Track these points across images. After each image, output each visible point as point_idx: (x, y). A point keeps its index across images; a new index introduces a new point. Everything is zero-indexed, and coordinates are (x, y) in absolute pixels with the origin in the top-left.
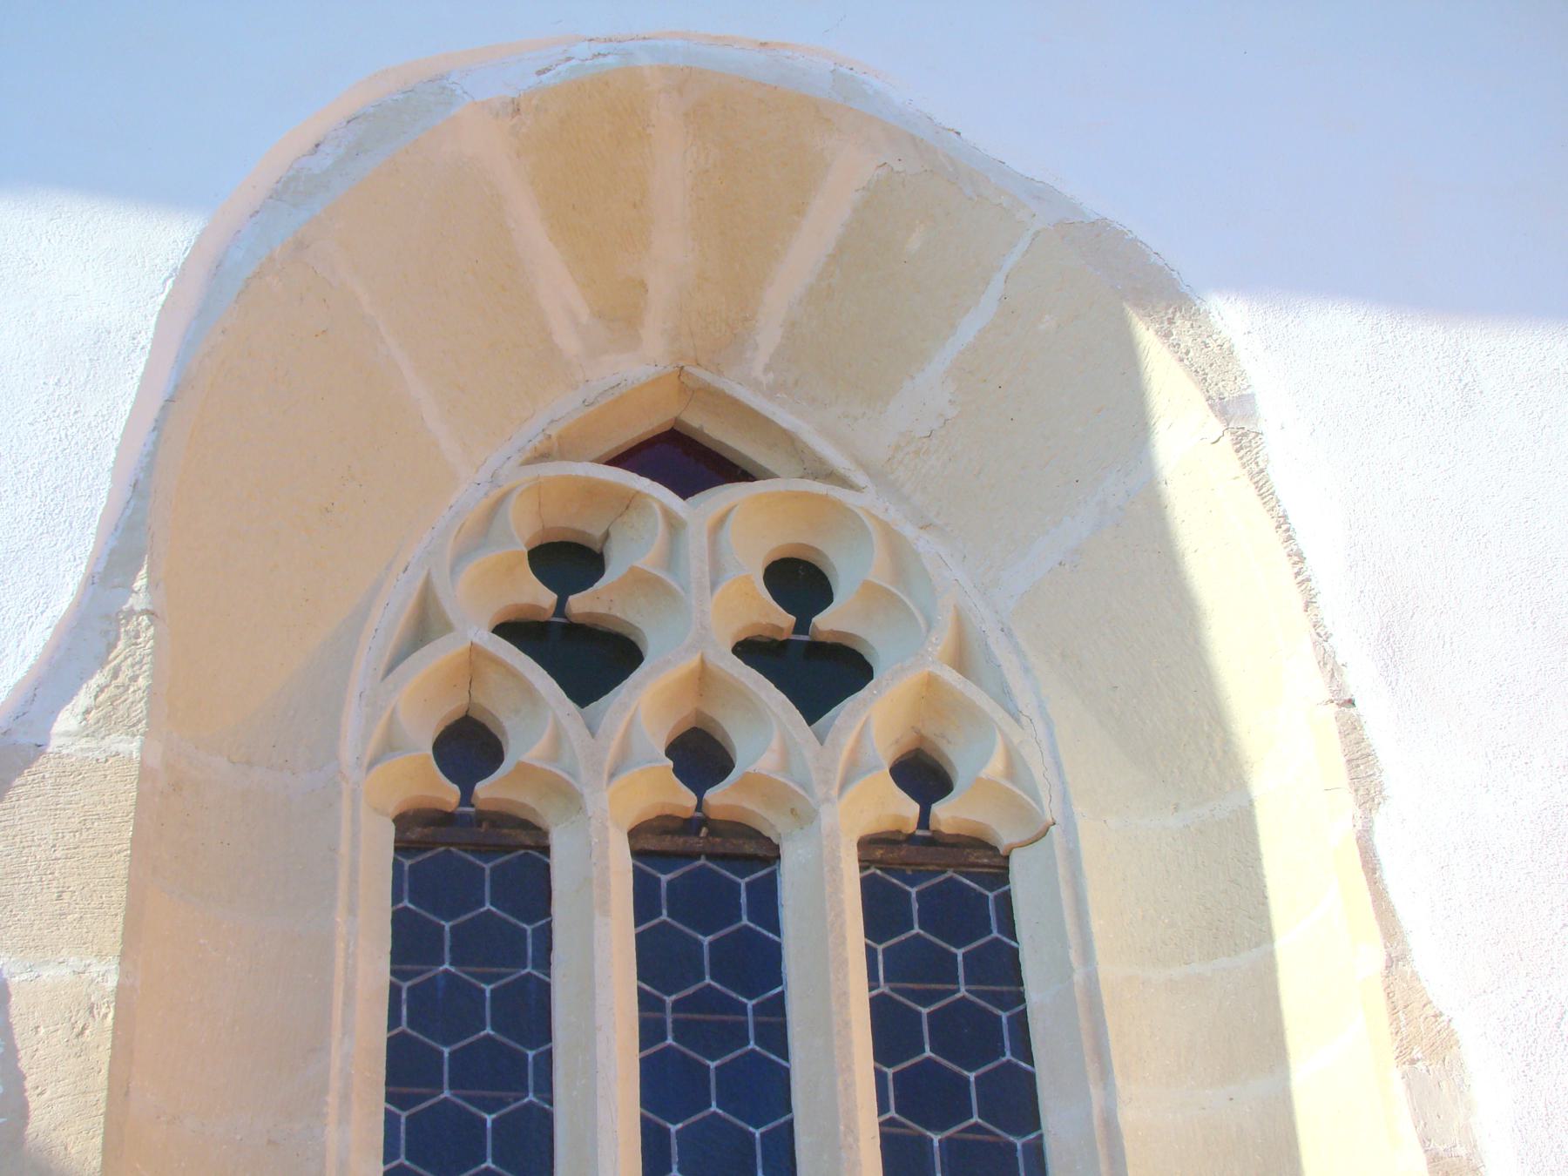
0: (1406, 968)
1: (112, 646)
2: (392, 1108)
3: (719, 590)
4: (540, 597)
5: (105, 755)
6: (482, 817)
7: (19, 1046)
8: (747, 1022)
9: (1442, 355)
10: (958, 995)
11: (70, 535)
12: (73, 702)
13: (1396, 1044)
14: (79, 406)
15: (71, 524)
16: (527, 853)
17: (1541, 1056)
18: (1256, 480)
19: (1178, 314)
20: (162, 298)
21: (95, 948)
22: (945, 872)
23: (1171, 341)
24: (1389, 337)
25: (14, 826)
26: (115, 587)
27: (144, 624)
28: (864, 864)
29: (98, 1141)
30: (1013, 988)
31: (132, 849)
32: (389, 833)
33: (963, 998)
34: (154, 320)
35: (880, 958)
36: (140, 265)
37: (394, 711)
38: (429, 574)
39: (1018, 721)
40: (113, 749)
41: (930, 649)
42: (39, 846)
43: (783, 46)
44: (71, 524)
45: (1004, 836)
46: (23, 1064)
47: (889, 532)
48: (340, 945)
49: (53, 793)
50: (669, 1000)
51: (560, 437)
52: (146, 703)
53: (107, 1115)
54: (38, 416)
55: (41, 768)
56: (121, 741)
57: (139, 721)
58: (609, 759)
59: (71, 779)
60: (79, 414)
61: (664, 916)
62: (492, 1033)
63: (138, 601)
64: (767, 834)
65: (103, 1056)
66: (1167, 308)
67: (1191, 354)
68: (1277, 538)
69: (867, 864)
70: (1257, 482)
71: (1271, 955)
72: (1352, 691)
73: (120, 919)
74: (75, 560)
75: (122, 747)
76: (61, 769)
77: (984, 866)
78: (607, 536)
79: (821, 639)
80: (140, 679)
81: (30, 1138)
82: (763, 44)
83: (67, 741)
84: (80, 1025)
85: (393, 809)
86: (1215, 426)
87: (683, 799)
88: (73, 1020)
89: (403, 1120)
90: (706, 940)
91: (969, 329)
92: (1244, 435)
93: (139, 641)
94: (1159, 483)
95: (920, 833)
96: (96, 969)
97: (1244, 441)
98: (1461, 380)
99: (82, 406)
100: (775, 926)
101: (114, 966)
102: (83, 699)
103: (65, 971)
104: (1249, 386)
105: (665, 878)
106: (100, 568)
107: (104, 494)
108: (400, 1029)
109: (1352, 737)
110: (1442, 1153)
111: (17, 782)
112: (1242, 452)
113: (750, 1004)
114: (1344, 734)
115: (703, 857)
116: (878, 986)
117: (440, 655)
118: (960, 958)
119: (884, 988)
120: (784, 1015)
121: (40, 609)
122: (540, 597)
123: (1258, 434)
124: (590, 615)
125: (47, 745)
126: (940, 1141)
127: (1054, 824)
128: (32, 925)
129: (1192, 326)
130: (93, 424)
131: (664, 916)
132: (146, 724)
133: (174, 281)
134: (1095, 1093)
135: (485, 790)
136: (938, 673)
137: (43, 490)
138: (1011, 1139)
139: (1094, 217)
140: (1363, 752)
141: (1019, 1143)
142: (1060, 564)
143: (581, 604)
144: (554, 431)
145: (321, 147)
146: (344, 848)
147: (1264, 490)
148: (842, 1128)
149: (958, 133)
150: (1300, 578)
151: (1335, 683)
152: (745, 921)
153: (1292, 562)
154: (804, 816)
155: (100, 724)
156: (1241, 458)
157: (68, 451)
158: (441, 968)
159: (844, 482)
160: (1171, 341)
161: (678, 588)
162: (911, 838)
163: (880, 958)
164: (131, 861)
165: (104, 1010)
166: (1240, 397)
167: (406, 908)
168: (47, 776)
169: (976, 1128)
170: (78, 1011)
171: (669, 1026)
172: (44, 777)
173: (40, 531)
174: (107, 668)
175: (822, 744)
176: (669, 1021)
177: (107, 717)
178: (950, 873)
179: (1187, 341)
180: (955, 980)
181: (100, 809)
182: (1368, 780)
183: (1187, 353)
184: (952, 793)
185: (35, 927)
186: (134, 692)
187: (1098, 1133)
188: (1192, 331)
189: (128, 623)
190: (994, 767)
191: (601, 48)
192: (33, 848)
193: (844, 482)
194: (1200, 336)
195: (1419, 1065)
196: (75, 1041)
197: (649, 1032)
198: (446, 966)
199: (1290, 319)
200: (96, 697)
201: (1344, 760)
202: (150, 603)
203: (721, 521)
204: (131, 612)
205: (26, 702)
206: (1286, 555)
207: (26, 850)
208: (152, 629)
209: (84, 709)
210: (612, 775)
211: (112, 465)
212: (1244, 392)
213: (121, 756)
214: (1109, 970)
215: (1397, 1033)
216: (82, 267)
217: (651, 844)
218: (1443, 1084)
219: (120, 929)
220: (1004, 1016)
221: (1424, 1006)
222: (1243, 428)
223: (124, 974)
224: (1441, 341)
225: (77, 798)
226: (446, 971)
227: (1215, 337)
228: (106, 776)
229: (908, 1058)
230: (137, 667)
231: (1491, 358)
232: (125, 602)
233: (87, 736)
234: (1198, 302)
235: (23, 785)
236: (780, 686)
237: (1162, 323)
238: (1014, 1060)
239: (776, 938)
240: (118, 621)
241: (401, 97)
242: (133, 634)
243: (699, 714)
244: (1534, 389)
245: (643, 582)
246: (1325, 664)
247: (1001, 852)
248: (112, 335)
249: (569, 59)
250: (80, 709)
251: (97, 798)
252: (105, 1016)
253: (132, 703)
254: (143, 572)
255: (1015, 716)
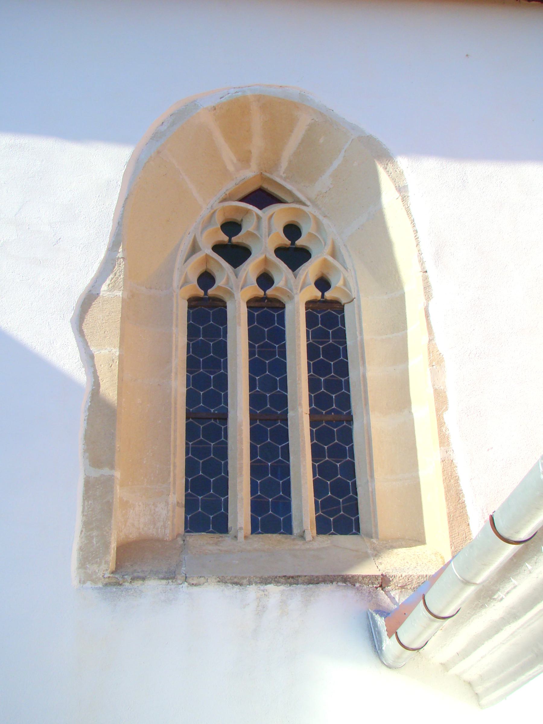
0: (434, 342)
1: (114, 267)
2: (188, 374)
3: (270, 236)
4: (224, 238)
5: (114, 296)
6: (210, 298)
7: (97, 370)
8: (276, 351)
9: (458, 172)
10: (330, 342)
11: (103, 238)
12: (105, 282)
13: (429, 362)
14: (104, 202)
15: (103, 235)
16: (221, 308)
17: (464, 363)
18: (407, 209)
19: (389, 162)
20: (124, 171)
21: (113, 345)
22: (328, 310)
23: (387, 170)
24: (445, 167)
25: (93, 315)
26: (114, 251)
27: (122, 261)
28: (307, 309)
29: (116, 392)
30: (344, 340)
31: (121, 320)
32: (186, 304)
33: (331, 343)
34: (122, 177)
35: (310, 333)
36: (118, 162)
37: (186, 274)
38: (195, 235)
39: (347, 270)
40: (115, 295)
41: (325, 251)
42: (99, 320)
43: (286, 87)
44: (103, 235)
45: (343, 301)
46: (98, 374)
47: (315, 217)
48: (174, 335)
49: (102, 306)
50: (257, 345)
51: (229, 194)
52: (123, 282)
53: (118, 386)
54: (94, 206)
55: (99, 300)
56: (117, 292)
57: (121, 287)
58: (241, 284)
59: (106, 303)
60: (104, 205)
61: (256, 324)
62: (212, 355)
63: (120, 255)
64: (282, 301)
65: (116, 372)
66: (387, 160)
67: (392, 174)
68: (411, 226)
69: (307, 308)
70: (407, 210)
71: (406, 333)
72: (427, 269)
73: (119, 338)
74: (104, 245)
75: (118, 294)
76: (103, 300)
77: (337, 308)
78: (242, 220)
79: (298, 247)
80: (121, 276)
81: (101, 392)
82: (281, 87)
83: (104, 292)
84: (111, 364)
85: (187, 298)
86: (397, 194)
87: (261, 293)
88: (109, 363)
89: (191, 377)
90: (266, 330)
91: (336, 164)
92: (405, 197)
93: (121, 265)
94: (383, 209)
95: (322, 299)
96: (114, 350)
97: (404, 199)
98: (463, 179)
99: (105, 202)
100: (284, 326)
101: (118, 350)
102: (108, 282)
103: (107, 351)
104: (407, 183)
105: (256, 314)
106: (111, 246)
107: (111, 226)
108: (190, 354)
109: (426, 281)
110: (437, 388)
111: (93, 303)
112: (404, 202)
113: (277, 346)
114: (423, 280)
115: (266, 308)
116: (309, 341)
117: (198, 257)
118: (331, 333)
119: (311, 341)
120: (286, 349)
121: (97, 259)
122: (224, 238)
123: (408, 196)
124: (238, 242)
125: (100, 294)
126: (323, 380)
127: (355, 298)
128: (99, 340)
129: (393, 166)
130: (108, 207)
131: (256, 324)
132: (123, 288)
133: (127, 166)
134: (361, 369)
135: (211, 292)
136: (327, 258)
137: (96, 226)
138: (341, 379)
139: (368, 135)
140: (428, 285)
141: (343, 380)
142: (359, 229)
143: (235, 239)
144: (227, 193)
145: (164, 123)
146: (174, 310)
147: (409, 212)
148: (297, 379)
149: (333, 111)
150: (416, 237)
151: (422, 267)
152: (276, 324)
153: (414, 233)
154: (291, 298)
155: (112, 288)
156: (403, 203)
157: (102, 215)
158: (200, 338)
159: (304, 204)
160: (387, 170)
161: (259, 236)
162: (319, 301)
163: (310, 333)
164: (121, 323)
165: (116, 361)
166: (404, 186)
167: (191, 323)
168: (100, 302)
169: (333, 376)
170: (110, 361)
171: (257, 352)
172: (99, 302)
173: (96, 237)
174: (113, 273)
175: (296, 278)
176: (257, 351)
177: (114, 286)
178: (329, 310)
179: (391, 170)
180: (329, 338)
181: (113, 310)
182: (429, 292)
183: (391, 174)
184: (331, 288)
185: (99, 340)
186: (120, 279)
187: (361, 378)
188: (392, 167)
189: (118, 261)
190: (340, 283)
191: (236, 90)
192: (98, 320)
193: (304, 204)
194: (395, 168)
195: (434, 367)
196: (110, 368)
197: (251, 353)
198: (201, 338)
199: (419, 163)
200: (111, 281)
201: (423, 287)
202: (123, 255)
203: (271, 217)
204: (119, 258)
205: (95, 283)
206: (413, 231)
207: (96, 321)
208: (124, 262)
209: (108, 284)
210: (242, 288)
211: (112, 218)
212: (405, 185)
213: (117, 296)
214: (367, 337)
215: (430, 359)
216: (104, 164)
217: (252, 305)
218: (440, 371)
219: (119, 340)
220: (341, 347)
221: (437, 352)
222: (404, 195)
223: (120, 351)
224: (458, 168)
225: (108, 307)
226: (201, 339)
227: (399, 168)
228: (114, 301)
229: (316, 359)
230: (120, 273)
231: (471, 172)
232: (117, 255)
233: (109, 291)
234: (395, 159)
235: (95, 304)
236: (285, 263)
237: (385, 165)
238: (343, 359)
239: (284, 329)
240: (115, 260)
241: (185, 107)
242: (119, 264)
243: (265, 269)
244: (482, 181)
245: (250, 234)
246: (420, 261)
247: (342, 304)
248: (112, 182)
249: (228, 94)
250: (107, 284)
251: (112, 307)
252: (116, 362)
253: (120, 282)
254: (121, 247)
255: (346, 269)
